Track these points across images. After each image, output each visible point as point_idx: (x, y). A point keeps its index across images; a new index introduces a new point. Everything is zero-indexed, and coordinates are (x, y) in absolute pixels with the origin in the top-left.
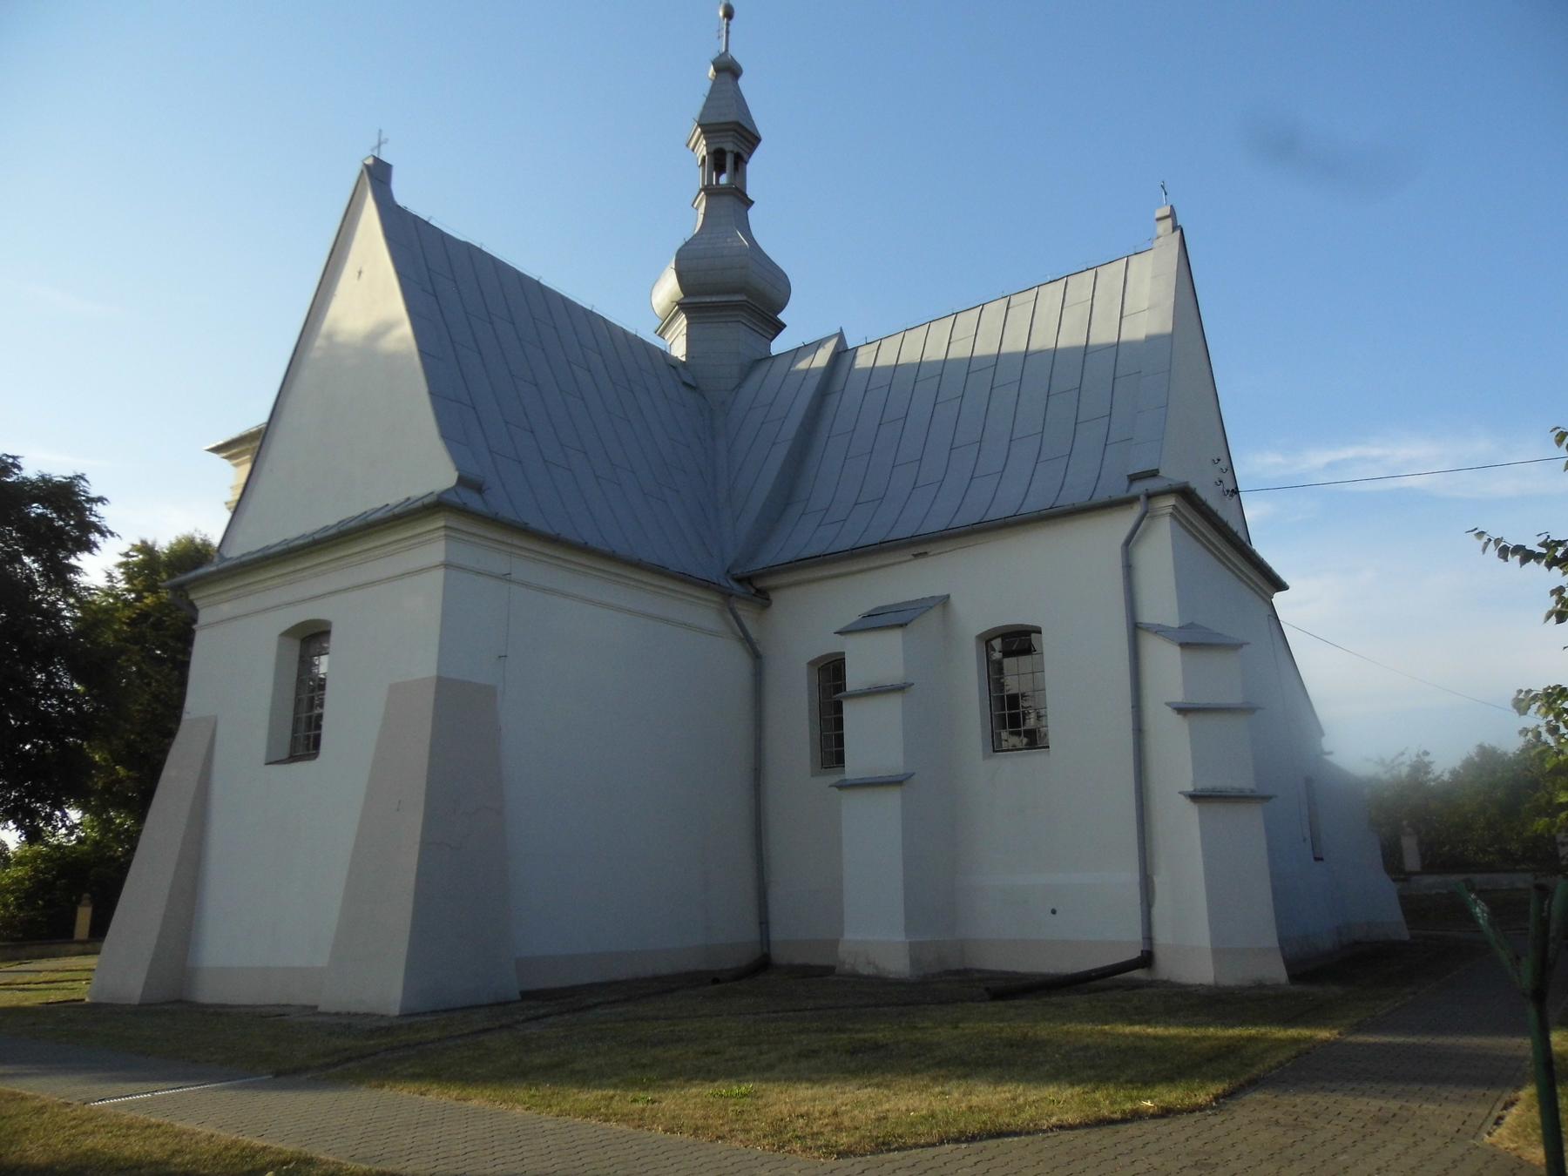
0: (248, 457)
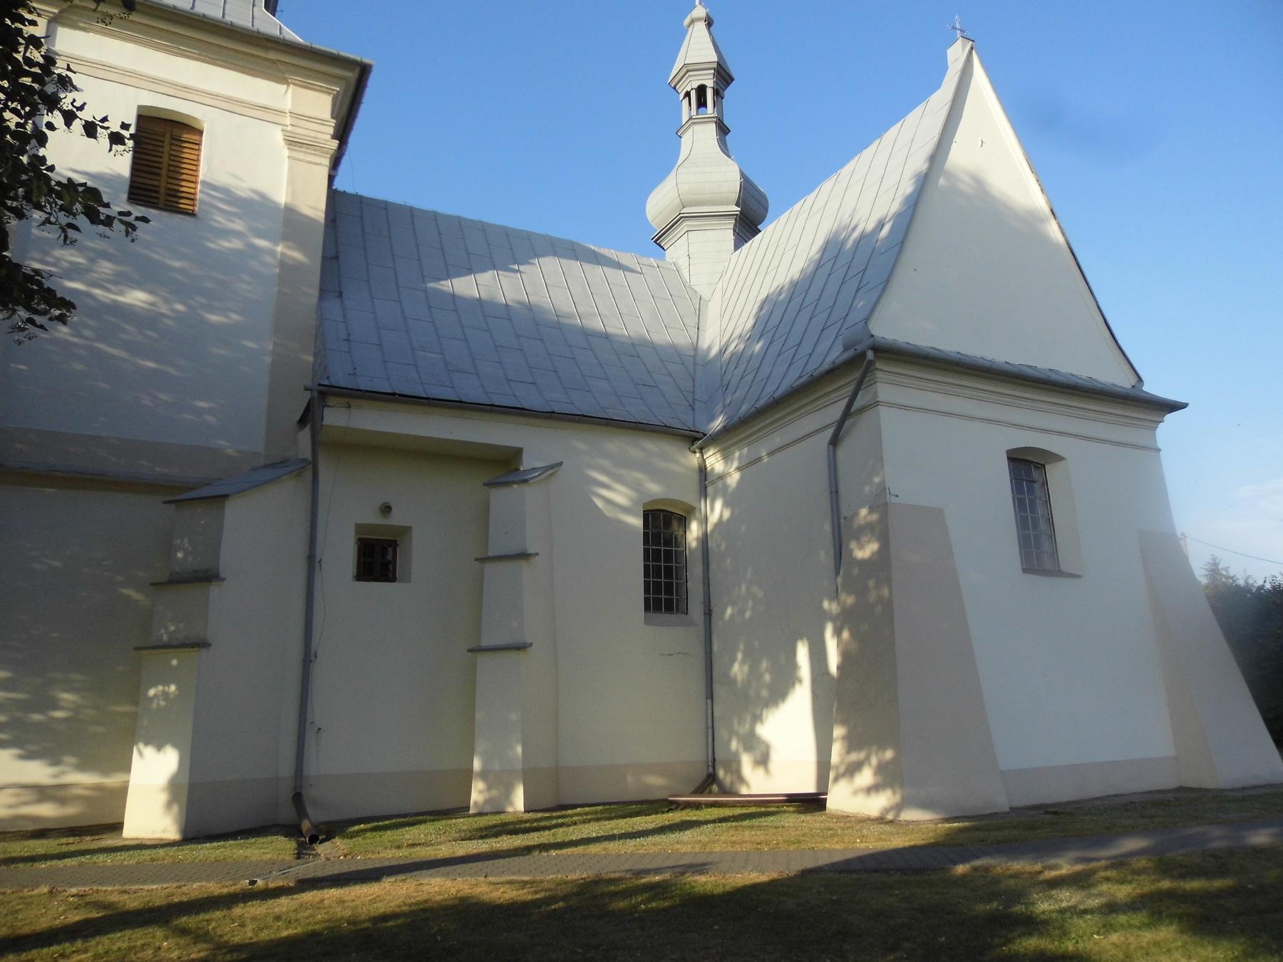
0: (56, 11)
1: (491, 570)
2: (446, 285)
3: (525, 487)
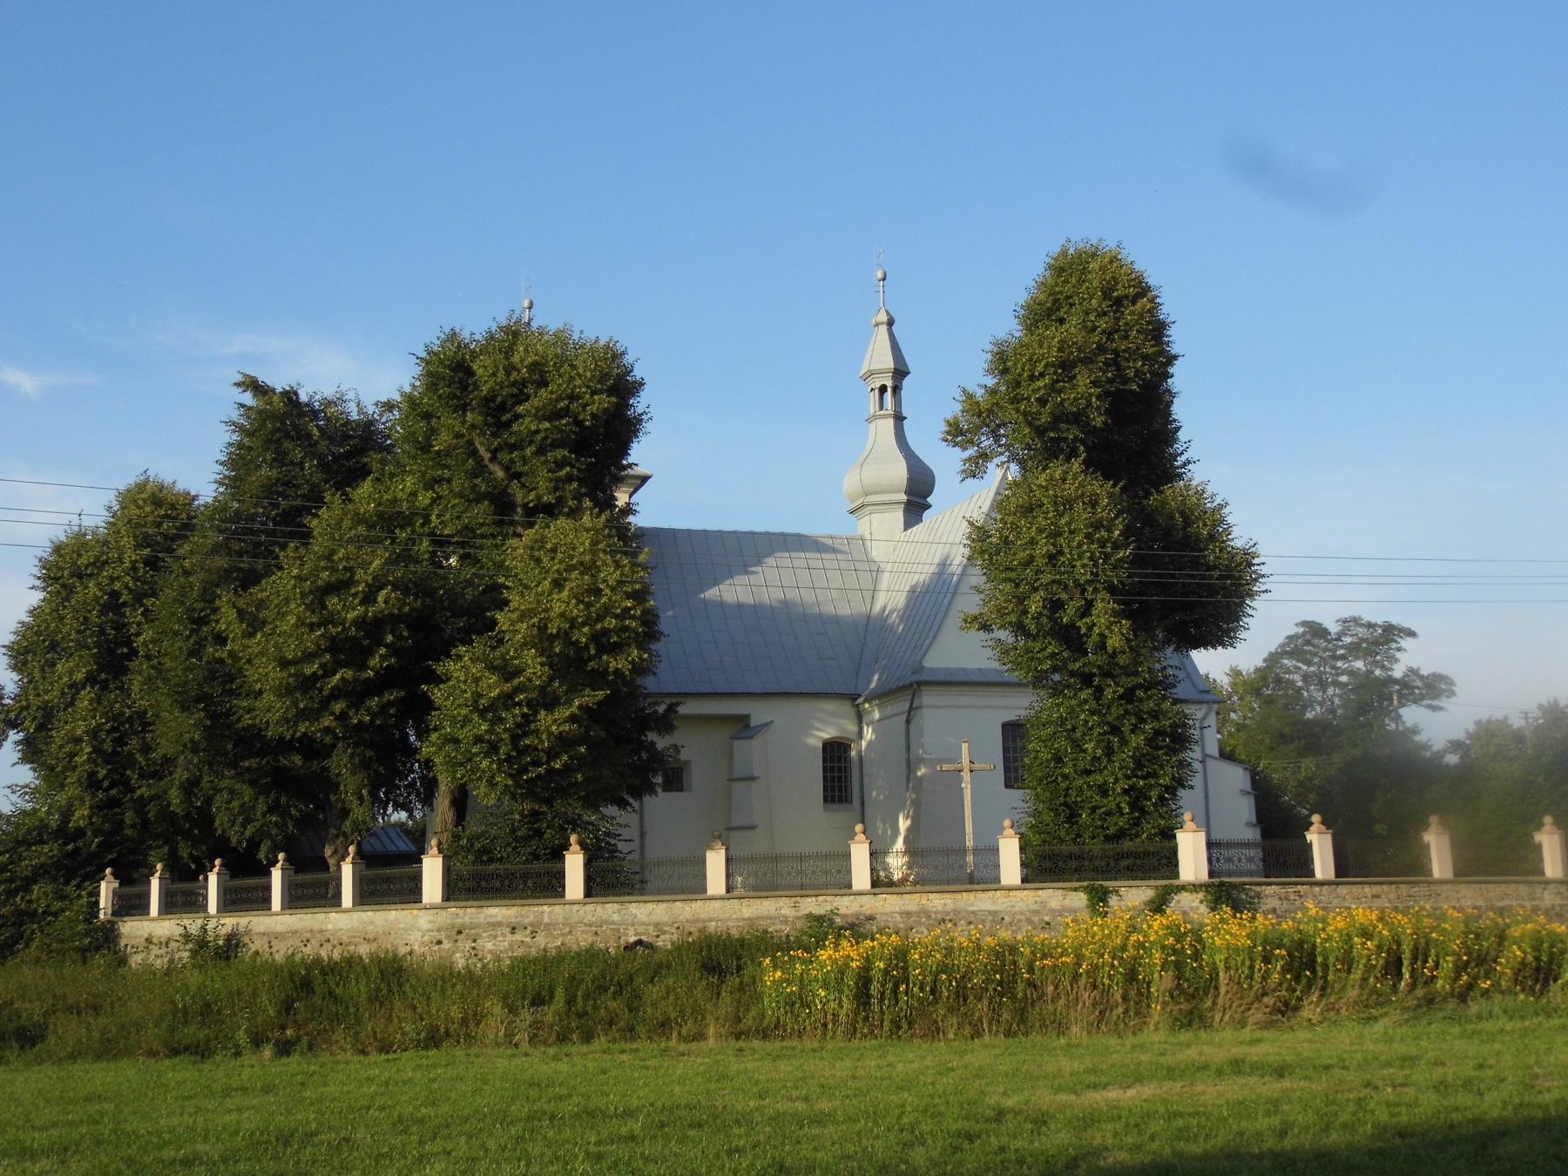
1: (735, 785)
2: (712, 594)
3: (752, 740)
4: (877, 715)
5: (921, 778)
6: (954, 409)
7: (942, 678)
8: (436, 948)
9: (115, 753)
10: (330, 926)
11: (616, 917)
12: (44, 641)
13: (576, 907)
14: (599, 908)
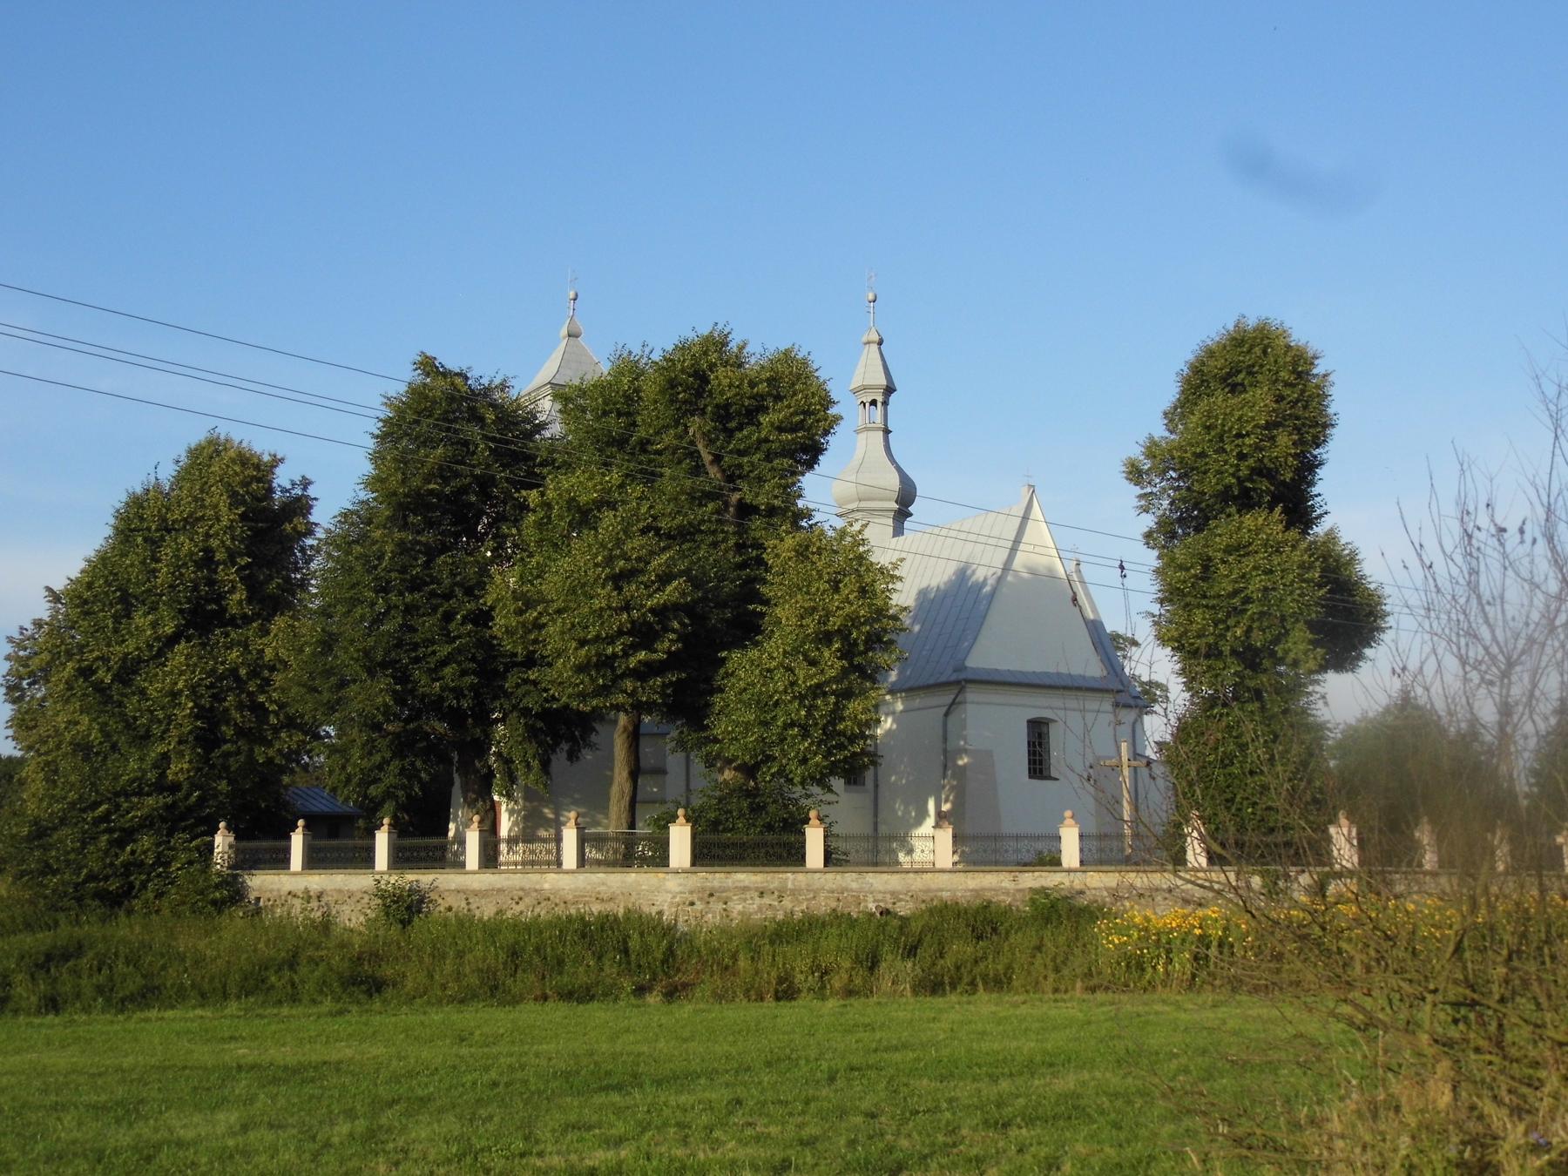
4: (899, 706)
5: (965, 766)
6: (1136, 452)
7: (985, 677)
8: (689, 909)
9: (212, 709)
10: (546, 886)
11: (854, 885)
12: (115, 592)
13: (818, 875)
14: (839, 877)
